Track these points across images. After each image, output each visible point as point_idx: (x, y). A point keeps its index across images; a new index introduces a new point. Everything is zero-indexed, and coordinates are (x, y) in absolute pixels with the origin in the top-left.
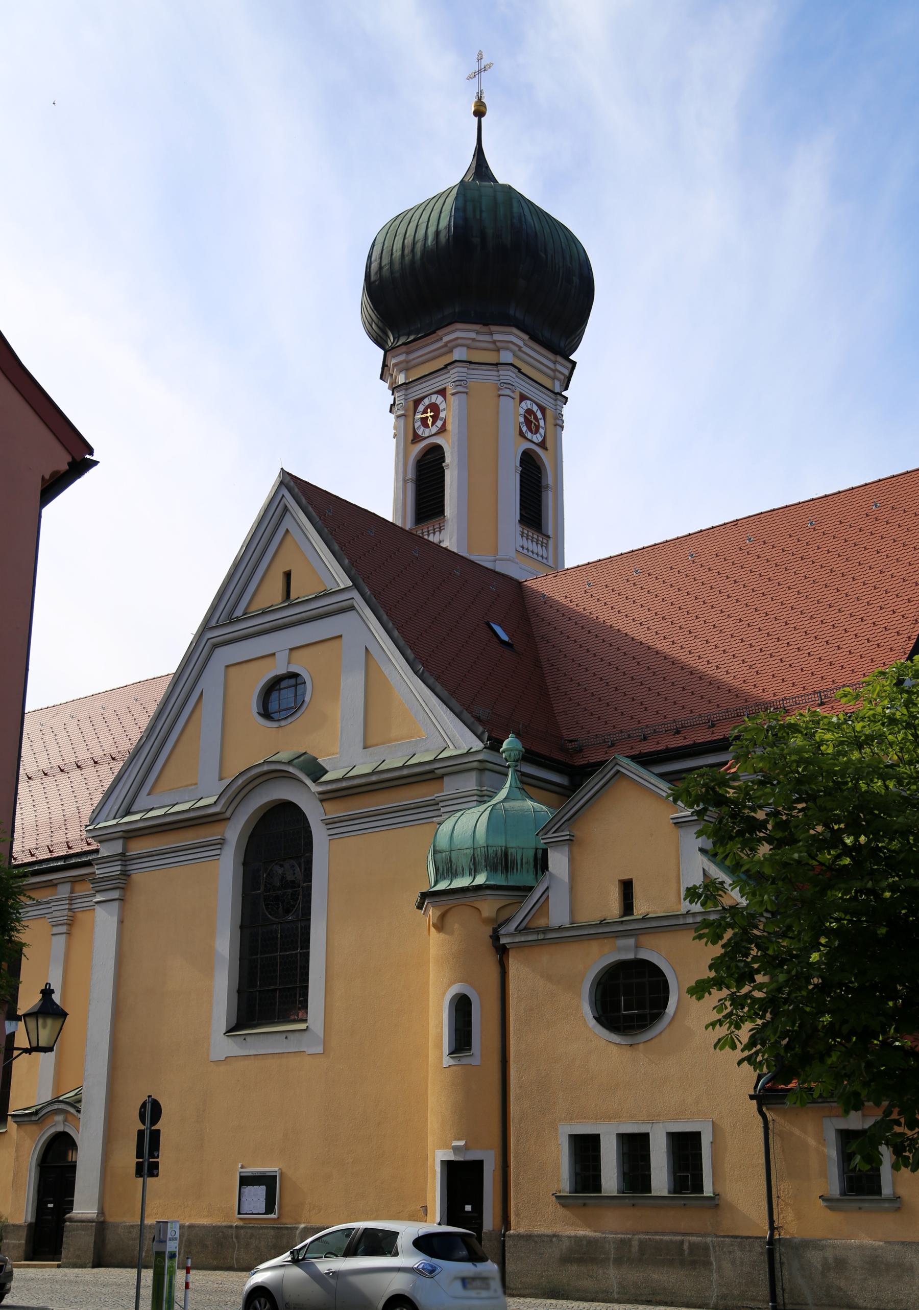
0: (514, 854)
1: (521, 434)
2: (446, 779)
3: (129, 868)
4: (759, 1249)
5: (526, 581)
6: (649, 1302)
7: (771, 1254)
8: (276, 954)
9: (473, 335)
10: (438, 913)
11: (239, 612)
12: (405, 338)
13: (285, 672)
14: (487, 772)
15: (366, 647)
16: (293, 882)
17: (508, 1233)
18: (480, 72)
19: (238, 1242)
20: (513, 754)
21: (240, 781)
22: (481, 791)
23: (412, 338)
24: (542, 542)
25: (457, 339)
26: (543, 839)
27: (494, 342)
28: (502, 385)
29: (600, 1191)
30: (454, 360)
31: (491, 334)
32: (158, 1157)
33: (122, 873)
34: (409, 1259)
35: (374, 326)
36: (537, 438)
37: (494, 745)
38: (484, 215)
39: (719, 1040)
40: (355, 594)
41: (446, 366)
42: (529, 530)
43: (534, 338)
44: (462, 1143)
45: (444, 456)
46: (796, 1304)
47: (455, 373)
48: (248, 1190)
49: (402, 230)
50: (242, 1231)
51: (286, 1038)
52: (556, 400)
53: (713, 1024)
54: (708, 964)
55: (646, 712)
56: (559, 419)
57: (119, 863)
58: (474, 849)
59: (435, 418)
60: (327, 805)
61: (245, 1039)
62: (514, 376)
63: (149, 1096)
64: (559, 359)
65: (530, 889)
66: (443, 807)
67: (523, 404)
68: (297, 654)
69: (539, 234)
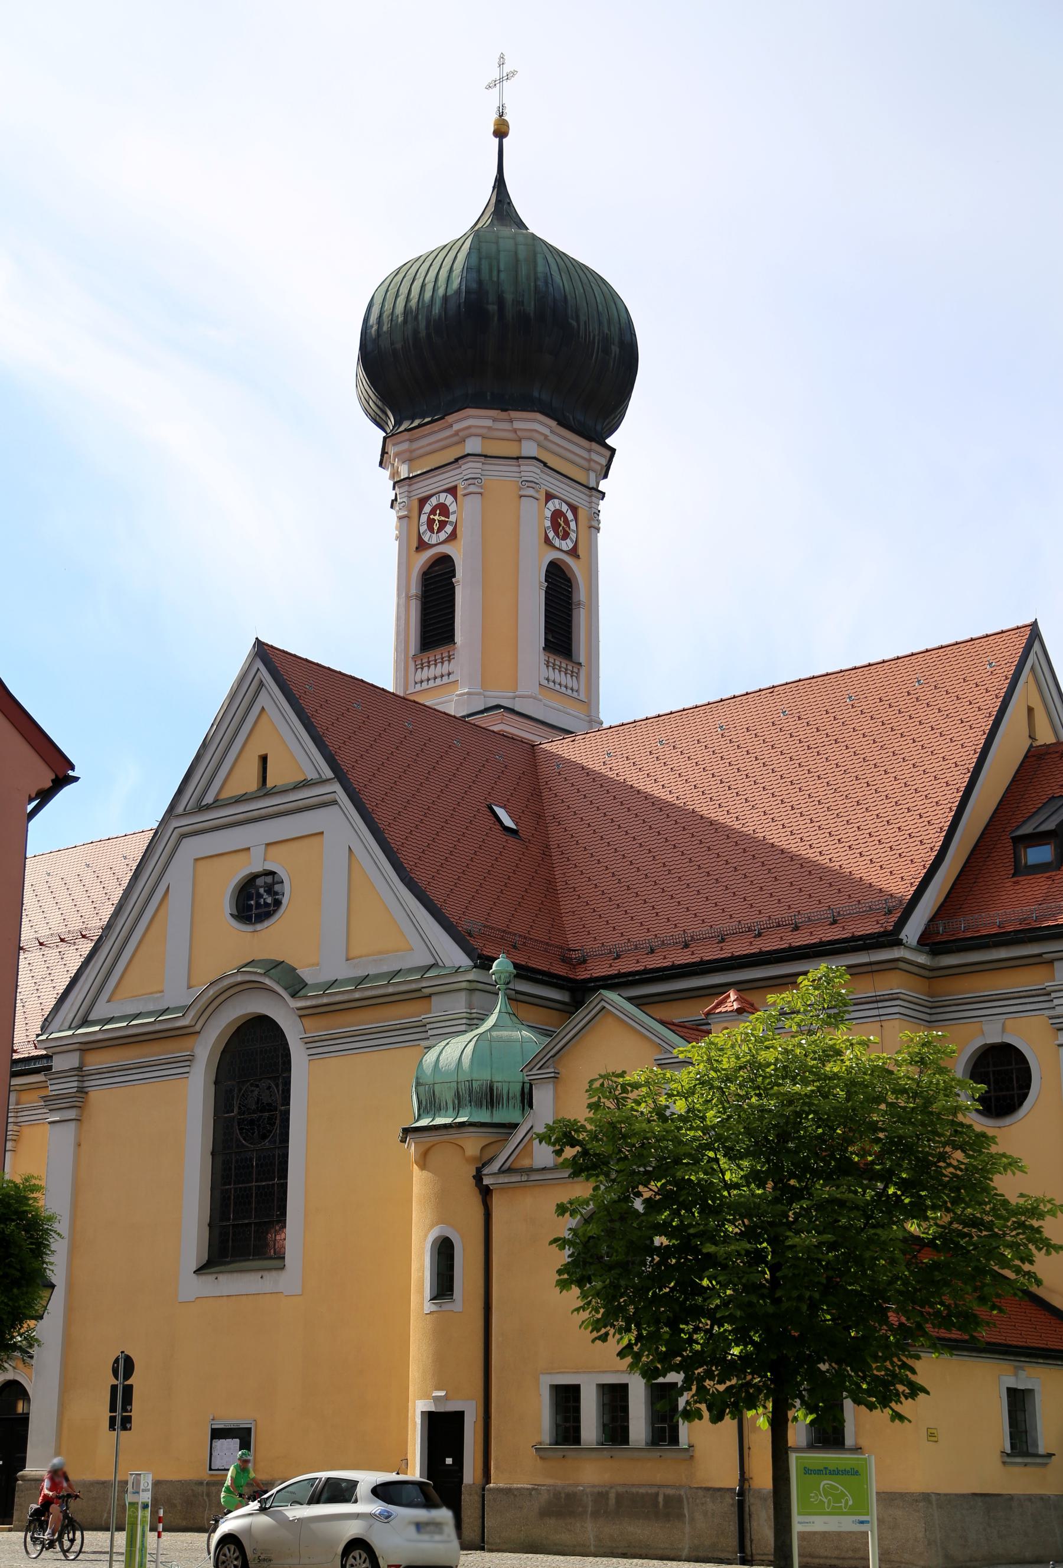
0: (500, 1088)
1: (547, 541)
2: (434, 999)
3: (86, 1084)
4: (731, 1501)
5: (540, 744)
6: (624, 1556)
7: (741, 1505)
8: (251, 1185)
9: (489, 423)
10: (422, 1149)
11: (209, 799)
12: (409, 422)
13: (261, 870)
14: (477, 992)
15: (349, 847)
16: (269, 1105)
17: (487, 1486)
18: (501, 80)
19: (209, 1500)
20: (503, 977)
21: (211, 992)
22: (471, 1013)
23: (416, 423)
24: (572, 672)
25: (469, 427)
26: (527, 1076)
27: (515, 431)
28: (523, 483)
29: (628, 1444)
30: (466, 453)
31: (511, 421)
32: (131, 1411)
33: (79, 1089)
34: (366, 1506)
35: (371, 403)
36: (567, 545)
37: (484, 962)
38: (503, 276)
39: (583, 1322)
40: (337, 787)
41: (457, 460)
42: (555, 657)
43: (561, 424)
44: (442, 1393)
45: (455, 569)
46: (762, 1555)
47: (469, 468)
48: (219, 1444)
49: (404, 291)
50: (213, 1488)
51: (262, 1277)
52: (590, 496)
53: (578, 1310)
54: (557, 1268)
55: (657, 917)
56: (594, 520)
57: (76, 1078)
58: (458, 1083)
59: (443, 525)
60: (307, 1022)
61: (216, 1278)
62: (538, 471)
63: (122, 1352)
64: (595, 446)
65: (515, 1126)
66: (430, 1029)
67: (550, 504)
68: (273, 850)
69: (569, 297)
